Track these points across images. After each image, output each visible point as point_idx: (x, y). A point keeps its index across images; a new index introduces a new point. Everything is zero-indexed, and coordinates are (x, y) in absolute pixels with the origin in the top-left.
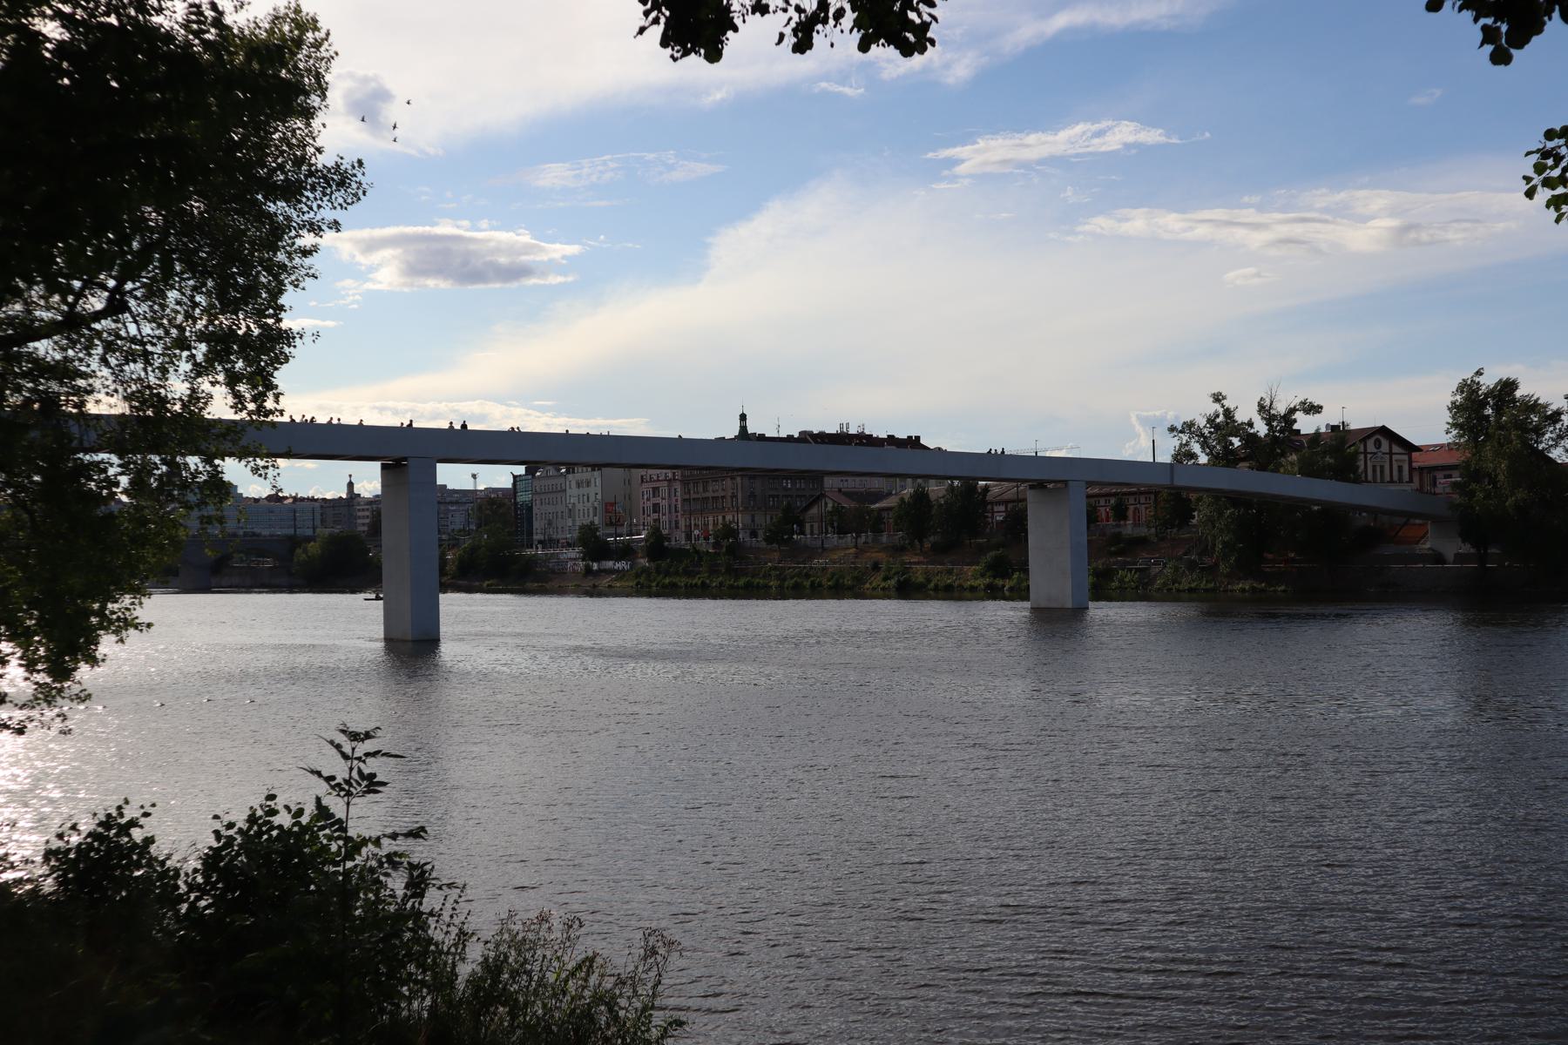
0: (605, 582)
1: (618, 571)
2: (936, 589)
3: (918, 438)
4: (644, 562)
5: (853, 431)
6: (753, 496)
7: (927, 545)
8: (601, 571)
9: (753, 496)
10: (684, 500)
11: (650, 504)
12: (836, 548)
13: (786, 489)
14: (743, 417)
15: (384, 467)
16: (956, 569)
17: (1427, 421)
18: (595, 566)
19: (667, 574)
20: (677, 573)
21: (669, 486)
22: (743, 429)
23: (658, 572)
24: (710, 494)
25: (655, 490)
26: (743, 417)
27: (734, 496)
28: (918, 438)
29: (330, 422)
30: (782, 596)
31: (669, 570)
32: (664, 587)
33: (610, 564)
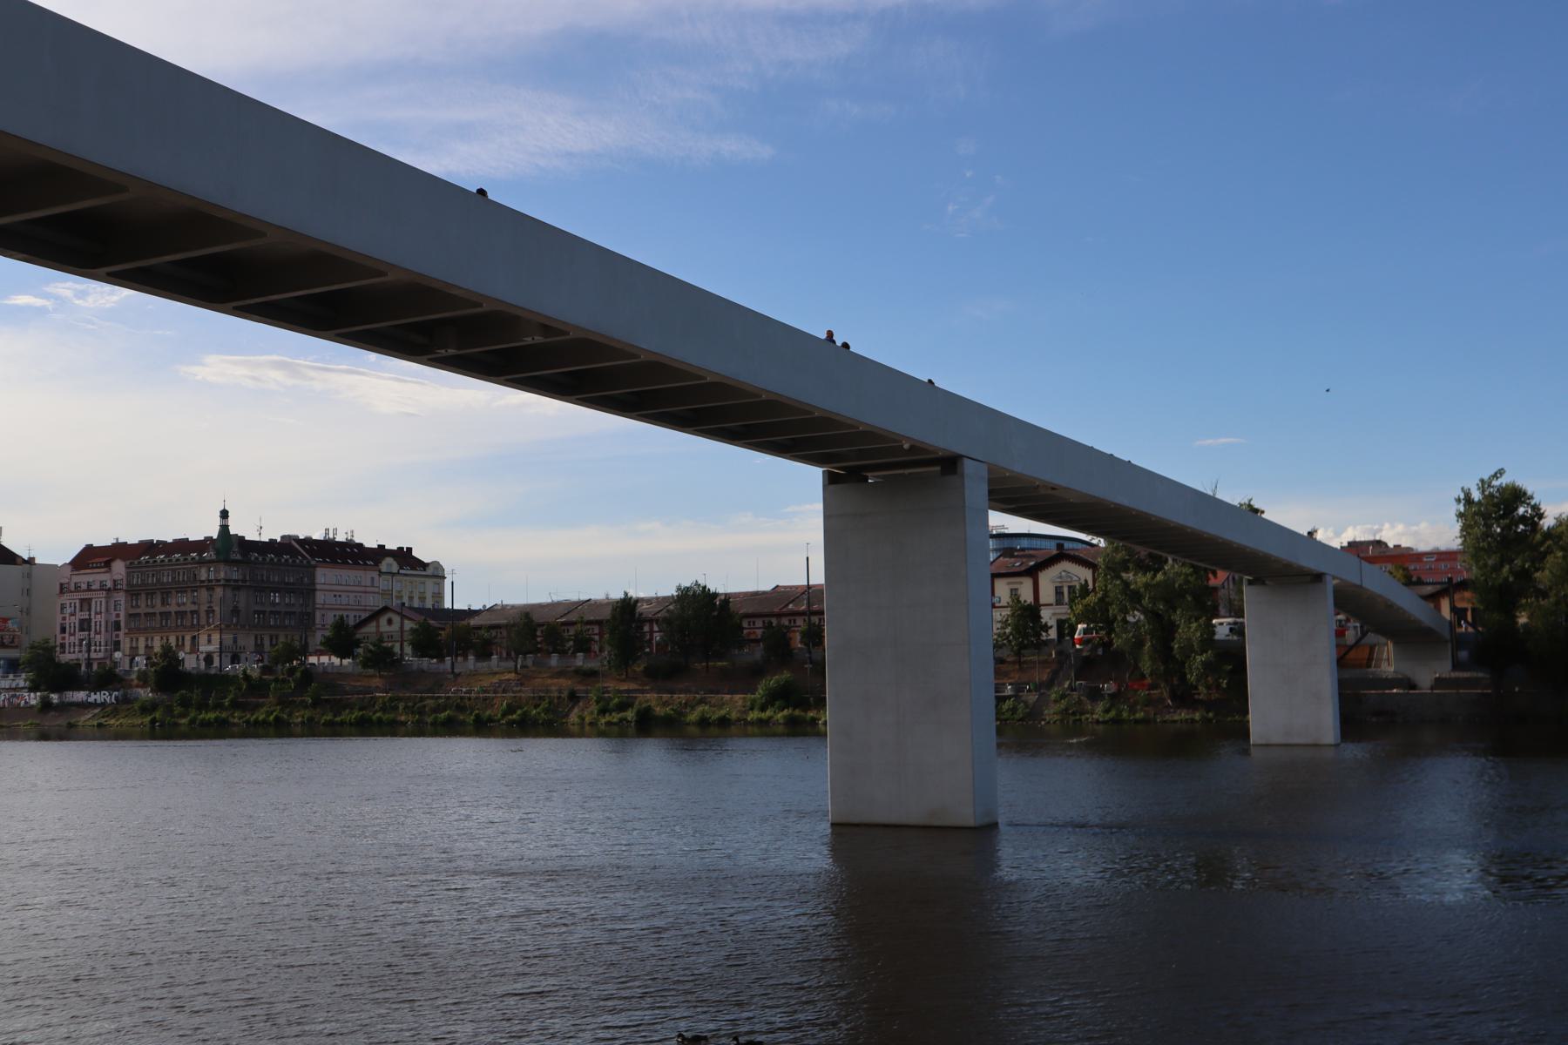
0: (85, 719)
1: (95, 705)
2: (434, 724)
3: (410, 549)
4: (145, 694)
5: (341, 538)
6: (235, 611)
7: (639, 667)
8: (64, 707)
9: (235, 611)
10: (130, 616)
11: (75, 620)
12: (474, 674)
13: (274, 604)
14: (224, 514)
15: (831, 480)
16: (714, 698)
17: (1431, 528)
18: (55, 697)
19: (202, 706)
20: (219, 706)
21: (108, 598)
22: (224, 529)
23: (185, 703)
24: (173, 608)
25: (86, 603)
26: (224, 514)
27: (210, 611)
28: (410, 549)
29: (1460, 515)
30: (419, 731)
31: (184, 706)
32: (206, 724)
33: (80, 696)
